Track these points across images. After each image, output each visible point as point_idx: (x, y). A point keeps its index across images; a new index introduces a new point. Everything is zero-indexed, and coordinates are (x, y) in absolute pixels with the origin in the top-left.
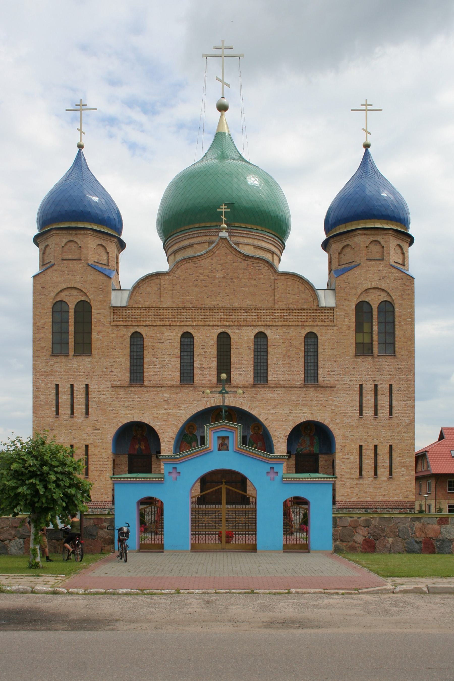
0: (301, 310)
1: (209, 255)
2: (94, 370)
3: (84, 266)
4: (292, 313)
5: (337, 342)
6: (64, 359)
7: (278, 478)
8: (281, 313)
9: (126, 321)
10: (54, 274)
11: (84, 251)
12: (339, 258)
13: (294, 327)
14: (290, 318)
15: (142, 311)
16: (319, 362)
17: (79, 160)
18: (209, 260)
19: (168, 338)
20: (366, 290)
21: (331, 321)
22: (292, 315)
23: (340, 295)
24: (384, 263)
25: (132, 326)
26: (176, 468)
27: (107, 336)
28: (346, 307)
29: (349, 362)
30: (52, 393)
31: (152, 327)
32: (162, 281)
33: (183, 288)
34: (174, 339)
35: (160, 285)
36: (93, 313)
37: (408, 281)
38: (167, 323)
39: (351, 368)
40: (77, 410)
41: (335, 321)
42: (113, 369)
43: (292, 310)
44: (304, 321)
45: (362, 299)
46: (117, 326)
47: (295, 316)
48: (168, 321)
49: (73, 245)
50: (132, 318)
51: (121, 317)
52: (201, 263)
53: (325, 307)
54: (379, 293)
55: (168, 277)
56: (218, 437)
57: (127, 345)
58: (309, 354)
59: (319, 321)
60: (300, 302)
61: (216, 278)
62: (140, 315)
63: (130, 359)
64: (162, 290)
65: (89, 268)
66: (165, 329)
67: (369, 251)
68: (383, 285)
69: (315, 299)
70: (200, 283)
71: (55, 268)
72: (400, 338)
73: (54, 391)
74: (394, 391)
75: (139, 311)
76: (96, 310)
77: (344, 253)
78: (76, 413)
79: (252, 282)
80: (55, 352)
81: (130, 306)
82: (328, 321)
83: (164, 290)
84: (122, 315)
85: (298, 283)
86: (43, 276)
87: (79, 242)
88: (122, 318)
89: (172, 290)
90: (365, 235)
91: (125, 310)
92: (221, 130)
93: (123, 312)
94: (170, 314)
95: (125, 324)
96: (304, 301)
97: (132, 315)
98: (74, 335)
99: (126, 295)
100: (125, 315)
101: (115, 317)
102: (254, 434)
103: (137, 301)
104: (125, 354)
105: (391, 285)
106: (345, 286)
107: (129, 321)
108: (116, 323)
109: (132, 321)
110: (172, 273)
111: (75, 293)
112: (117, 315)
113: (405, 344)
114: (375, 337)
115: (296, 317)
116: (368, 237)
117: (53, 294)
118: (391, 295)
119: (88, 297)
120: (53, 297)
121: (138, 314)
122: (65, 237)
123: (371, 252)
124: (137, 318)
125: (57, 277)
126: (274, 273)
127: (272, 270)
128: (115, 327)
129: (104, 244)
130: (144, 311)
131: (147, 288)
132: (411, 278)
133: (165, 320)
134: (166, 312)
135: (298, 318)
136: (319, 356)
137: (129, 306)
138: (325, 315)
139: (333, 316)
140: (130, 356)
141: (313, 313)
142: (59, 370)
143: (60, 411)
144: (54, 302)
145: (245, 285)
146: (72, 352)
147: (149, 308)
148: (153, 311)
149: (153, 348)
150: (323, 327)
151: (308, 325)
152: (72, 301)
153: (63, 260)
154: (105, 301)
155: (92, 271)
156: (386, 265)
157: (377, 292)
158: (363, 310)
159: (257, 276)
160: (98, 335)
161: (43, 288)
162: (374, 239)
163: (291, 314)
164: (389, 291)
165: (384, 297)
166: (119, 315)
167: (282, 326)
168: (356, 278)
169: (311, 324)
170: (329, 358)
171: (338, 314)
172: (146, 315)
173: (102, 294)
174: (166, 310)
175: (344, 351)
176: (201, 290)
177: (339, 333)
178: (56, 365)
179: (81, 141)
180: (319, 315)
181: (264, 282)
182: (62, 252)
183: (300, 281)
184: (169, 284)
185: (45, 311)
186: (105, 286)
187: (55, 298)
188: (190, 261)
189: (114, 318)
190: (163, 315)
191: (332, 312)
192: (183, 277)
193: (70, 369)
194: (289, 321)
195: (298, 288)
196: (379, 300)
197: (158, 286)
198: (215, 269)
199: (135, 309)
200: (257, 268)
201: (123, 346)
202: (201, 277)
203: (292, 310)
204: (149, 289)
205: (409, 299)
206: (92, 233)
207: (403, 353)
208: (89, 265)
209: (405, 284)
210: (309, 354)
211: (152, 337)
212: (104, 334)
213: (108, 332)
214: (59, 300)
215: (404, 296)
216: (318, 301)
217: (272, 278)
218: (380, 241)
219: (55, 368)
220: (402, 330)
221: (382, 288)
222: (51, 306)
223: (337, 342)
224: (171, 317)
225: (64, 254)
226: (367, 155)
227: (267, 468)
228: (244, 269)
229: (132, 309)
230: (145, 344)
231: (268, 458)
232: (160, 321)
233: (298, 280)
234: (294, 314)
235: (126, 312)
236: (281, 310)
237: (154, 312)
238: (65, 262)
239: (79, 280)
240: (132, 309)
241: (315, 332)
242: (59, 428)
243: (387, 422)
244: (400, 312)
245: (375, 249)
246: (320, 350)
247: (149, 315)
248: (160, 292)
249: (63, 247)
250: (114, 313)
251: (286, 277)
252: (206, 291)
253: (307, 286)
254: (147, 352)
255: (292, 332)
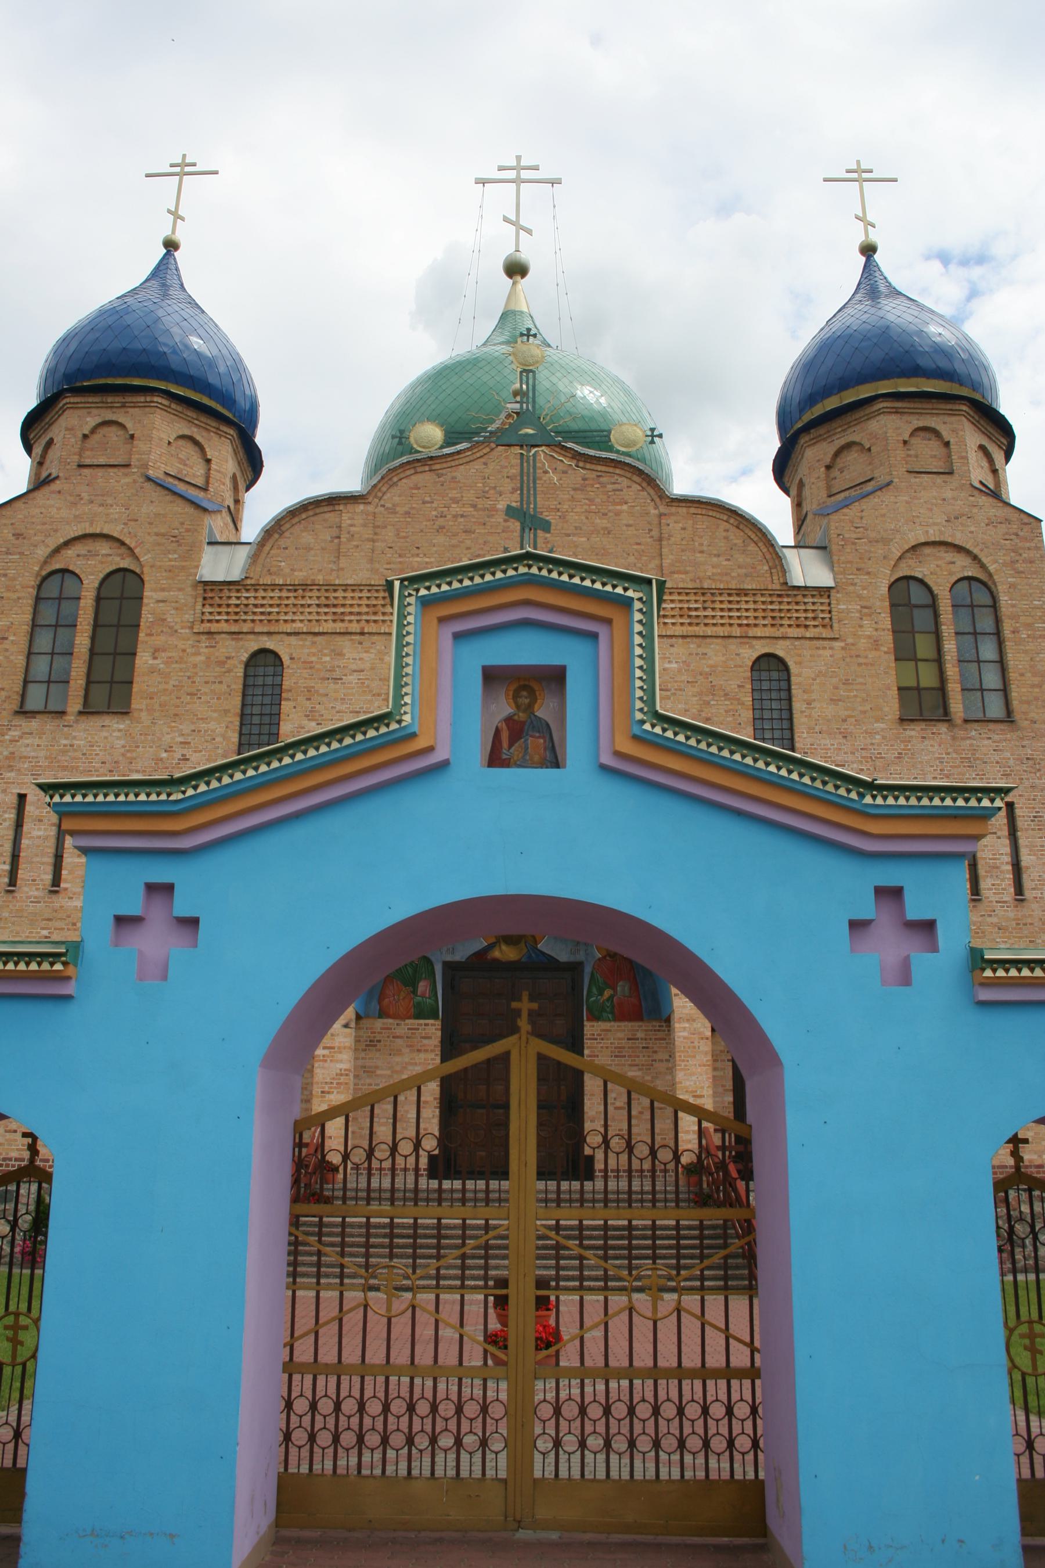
0: (738, 595)
1: (478, 455)
2: (134, 755)
3: (135, 481)
4: (713, 602)
5: (846, 683)
6: (50, 725)
7: (939, 968)
8: (681, 601)
9: (236, 621)
10: (51, 502)
11: (140, 445)
12: (829, 481)
13: (719, 641)
14: (705, 617)
15: (285, 594)
16: (797, 739)
17: (165, 273)
18: (478, 465)
19: (354, 667)
20: (914, 548)
21: (824, 626)
22: (713, 609)
23: (842, 558)
24: (954, 481)
25: (254, 633)
26: (169, 888)
27: (181, 660)
28: (864, 589)
29: (884, 738)
30: (5, 820)
31: (310, 638)
32: (345, 516)
33: (402, 534)
34: (373, 669)
35: (340, 527)
36: (145, 601)
37: (1026, 528)
38: (355, 627)
39: (892, 755)
40: (70, 872)
41: (836, 625)
42: (188, 753)
43: (713, 594)
44: (748, 625)
45: (903, 571)
46: (209, 633)
47: (722, 610)
48: (358, 621)
49: (112, 432)
50: (254, 613)
51: (224, 610)
52: (454, 474)
53: (806, 588)
54: (950, 556)
55: (362, 507)
56: (491, 676)
57: (233, 687)
58: (767, 715)
59: (790, 626)
60: (733, 574)
61: (497, 511)
62: (278, 605)
63: (242, 724)
64: (343, 540)
65: (148, 485)
66: (348, 643)
67: (912, 452)
68: (958, 535)
69: (775, 567)
70: (451, 523)
71: (56, 486)
72: (1022, 675)
73: (11, 816)
74: (1020, 823)
75: (277, 594)
76: (154, 590)
77: (841, 465)
78: (66, 882)
79: (598, 521)
80: (30, 706)
81: (253, 582)
82: (815, 626)
83: (349, 540)
84: (228, 606)
85: (724, 525)
86: (23, 506)
87: (129, 425)
88: (228, 613)
89: (373, 541)
90: (896, 412)
91: (238, 591)
92: (512, 307)
93: (229, 598)
94: (365, 602)
95: (234, 628)
96: (744, 571)
97: (256, 606)
98: (86, 657)
99: (242, 554)
100: (237, 606)
101: (208, 609)
102: (604, 957)
103: (273, 569)
104: (226, 711)
105: (980, 536)
106: (854, 536)
107: (245, 621)
108: (208, 625)
109: (253, 621)
110: (376, 496)
111: (104, 548)
112: (211, 605)
113: (1037, 690)
114: (952, 671)
115: (725, 614)
116: (906, 417)
117: (42, 552)
118: (984, 560)
119: (137, 559)
120: (42, 559)
121: (271, 602)
122: (95, 411)
123: (916, 456)
124: (270, 613)
125: (59, 509)
126: (658, 500)
127: (652, 492)
128: (203, 637)
129: (198, 438)
130: (291, 594)
131: (304, 534)
132: (1032, 520)
133: (347, 618)
134: (353, 598)
135: (730, 617)
136: (795, 720)
137: (249, 582)
138: (806, 611)
139: (830, 612)
140: (242, 715)
141: (772, 603)
142: (33, 754)
143: (21, 874)
144: (44, 573)
145: (576, 528)
146: (75, 705)
147: (305, 586)
148: (315, 594)
149: (310, 693)
150: (803, 641)
151: (759, 635)
152: (92, 567)
153: (80, 466)
154: (183, 568)
155: (156, 494)
156: (961, 487)
157: (942, 554)
158: (909, 599)
159: (610, 508)
160: (155, 658)
161: (18, 535)
162: (921, 424)
163: (708, 604)
164: (976, 551)
165: (963, 567)
166: (220, 606)
167: (683, 637)
168: (883, 516)
169: (769, 631)
170: (825, 728)
171: (842, 607)
172: (295, 605)
173: (175, 552)
174: (353, 591)
175: (868, 708)
176: (454, 542)
177: (848, 660)
178: (27, 741)
179: (174, 232)
180: (789, 610)
181: (631, 522)
182: (82, 449)
183: (732, 521)
184: (364, 525)
185: (15, 596)
186: (188, 530)
187: (45, 562)
188: (427, 468)
189: (203, 613)
190: (343, 605)
191: (827, 601)
192: (406, 509)
193: (64, 752)
194: (706, 625)
195: (726, 538)
196: (951, 574)
197: (335, 532)
198: (495, 488)
199: (265, 590)
200: (610, 487)
201: (224, 687)
202: (455, 509)
203: (713, 594)
204: (307, 538)
205: (1035, 573)
206: (166, 402)
207: (1032, 715)
208: (149, 479)
209: (1017, 535)
210: (767, 715)
211: (309, 665)
212: (170, 654)
213: (184, 651)
214: (58, 566)
215: (1018, 565)
216: (784, 572)
217: (653, 512)
218: (938, 428)
219: (23, 749)
220: (1025, 652)
221: (957, 543)
222: (33, 582)
223: (846, 683)
224: (365, 609)
225: (88, 453)
226: (870, 268)
227: (853, 888)
228: (575, 489)
229: (256, 590)
230: (286, 684)
231: (863, 814)
232: (334, 621)
233: (725, 518)
234: (718, 606)
235: (238, 598)
236: (679, 594)
237: (318, 598)
238: (86, 471)
239: (117, 516)
240: (256, 590)
241: (781, 653)
242: (13, 924)
243: (1011, 915)
244: (1013, 606)
245: (927, 451)
246: (798, 706)
247: (302, 605)
248: (339, 544)
249: (85, 436)
250: (205, 599)
251: (692, 510)
252: (468, 543)
253: (750, 533)
254: (291, 704)
255: (715, 654)
